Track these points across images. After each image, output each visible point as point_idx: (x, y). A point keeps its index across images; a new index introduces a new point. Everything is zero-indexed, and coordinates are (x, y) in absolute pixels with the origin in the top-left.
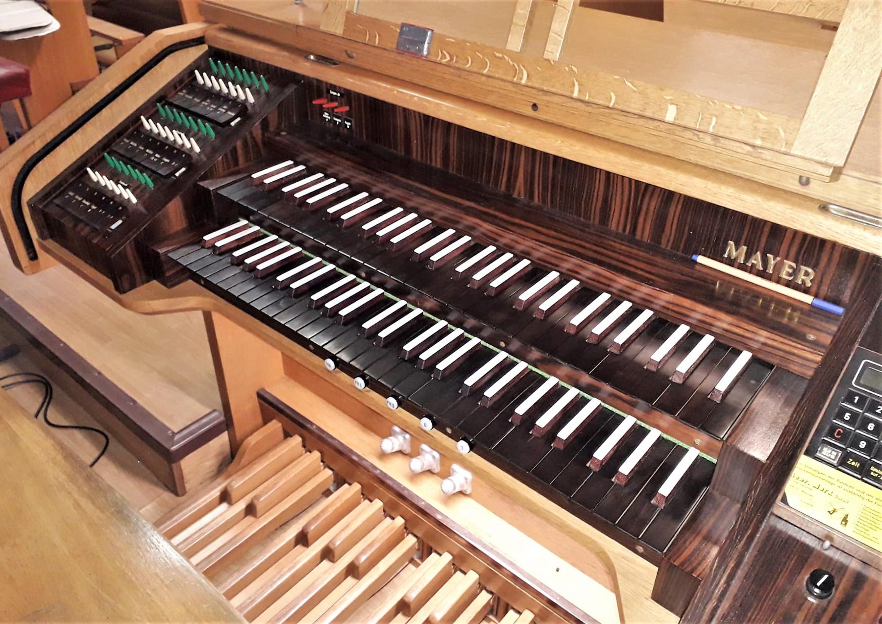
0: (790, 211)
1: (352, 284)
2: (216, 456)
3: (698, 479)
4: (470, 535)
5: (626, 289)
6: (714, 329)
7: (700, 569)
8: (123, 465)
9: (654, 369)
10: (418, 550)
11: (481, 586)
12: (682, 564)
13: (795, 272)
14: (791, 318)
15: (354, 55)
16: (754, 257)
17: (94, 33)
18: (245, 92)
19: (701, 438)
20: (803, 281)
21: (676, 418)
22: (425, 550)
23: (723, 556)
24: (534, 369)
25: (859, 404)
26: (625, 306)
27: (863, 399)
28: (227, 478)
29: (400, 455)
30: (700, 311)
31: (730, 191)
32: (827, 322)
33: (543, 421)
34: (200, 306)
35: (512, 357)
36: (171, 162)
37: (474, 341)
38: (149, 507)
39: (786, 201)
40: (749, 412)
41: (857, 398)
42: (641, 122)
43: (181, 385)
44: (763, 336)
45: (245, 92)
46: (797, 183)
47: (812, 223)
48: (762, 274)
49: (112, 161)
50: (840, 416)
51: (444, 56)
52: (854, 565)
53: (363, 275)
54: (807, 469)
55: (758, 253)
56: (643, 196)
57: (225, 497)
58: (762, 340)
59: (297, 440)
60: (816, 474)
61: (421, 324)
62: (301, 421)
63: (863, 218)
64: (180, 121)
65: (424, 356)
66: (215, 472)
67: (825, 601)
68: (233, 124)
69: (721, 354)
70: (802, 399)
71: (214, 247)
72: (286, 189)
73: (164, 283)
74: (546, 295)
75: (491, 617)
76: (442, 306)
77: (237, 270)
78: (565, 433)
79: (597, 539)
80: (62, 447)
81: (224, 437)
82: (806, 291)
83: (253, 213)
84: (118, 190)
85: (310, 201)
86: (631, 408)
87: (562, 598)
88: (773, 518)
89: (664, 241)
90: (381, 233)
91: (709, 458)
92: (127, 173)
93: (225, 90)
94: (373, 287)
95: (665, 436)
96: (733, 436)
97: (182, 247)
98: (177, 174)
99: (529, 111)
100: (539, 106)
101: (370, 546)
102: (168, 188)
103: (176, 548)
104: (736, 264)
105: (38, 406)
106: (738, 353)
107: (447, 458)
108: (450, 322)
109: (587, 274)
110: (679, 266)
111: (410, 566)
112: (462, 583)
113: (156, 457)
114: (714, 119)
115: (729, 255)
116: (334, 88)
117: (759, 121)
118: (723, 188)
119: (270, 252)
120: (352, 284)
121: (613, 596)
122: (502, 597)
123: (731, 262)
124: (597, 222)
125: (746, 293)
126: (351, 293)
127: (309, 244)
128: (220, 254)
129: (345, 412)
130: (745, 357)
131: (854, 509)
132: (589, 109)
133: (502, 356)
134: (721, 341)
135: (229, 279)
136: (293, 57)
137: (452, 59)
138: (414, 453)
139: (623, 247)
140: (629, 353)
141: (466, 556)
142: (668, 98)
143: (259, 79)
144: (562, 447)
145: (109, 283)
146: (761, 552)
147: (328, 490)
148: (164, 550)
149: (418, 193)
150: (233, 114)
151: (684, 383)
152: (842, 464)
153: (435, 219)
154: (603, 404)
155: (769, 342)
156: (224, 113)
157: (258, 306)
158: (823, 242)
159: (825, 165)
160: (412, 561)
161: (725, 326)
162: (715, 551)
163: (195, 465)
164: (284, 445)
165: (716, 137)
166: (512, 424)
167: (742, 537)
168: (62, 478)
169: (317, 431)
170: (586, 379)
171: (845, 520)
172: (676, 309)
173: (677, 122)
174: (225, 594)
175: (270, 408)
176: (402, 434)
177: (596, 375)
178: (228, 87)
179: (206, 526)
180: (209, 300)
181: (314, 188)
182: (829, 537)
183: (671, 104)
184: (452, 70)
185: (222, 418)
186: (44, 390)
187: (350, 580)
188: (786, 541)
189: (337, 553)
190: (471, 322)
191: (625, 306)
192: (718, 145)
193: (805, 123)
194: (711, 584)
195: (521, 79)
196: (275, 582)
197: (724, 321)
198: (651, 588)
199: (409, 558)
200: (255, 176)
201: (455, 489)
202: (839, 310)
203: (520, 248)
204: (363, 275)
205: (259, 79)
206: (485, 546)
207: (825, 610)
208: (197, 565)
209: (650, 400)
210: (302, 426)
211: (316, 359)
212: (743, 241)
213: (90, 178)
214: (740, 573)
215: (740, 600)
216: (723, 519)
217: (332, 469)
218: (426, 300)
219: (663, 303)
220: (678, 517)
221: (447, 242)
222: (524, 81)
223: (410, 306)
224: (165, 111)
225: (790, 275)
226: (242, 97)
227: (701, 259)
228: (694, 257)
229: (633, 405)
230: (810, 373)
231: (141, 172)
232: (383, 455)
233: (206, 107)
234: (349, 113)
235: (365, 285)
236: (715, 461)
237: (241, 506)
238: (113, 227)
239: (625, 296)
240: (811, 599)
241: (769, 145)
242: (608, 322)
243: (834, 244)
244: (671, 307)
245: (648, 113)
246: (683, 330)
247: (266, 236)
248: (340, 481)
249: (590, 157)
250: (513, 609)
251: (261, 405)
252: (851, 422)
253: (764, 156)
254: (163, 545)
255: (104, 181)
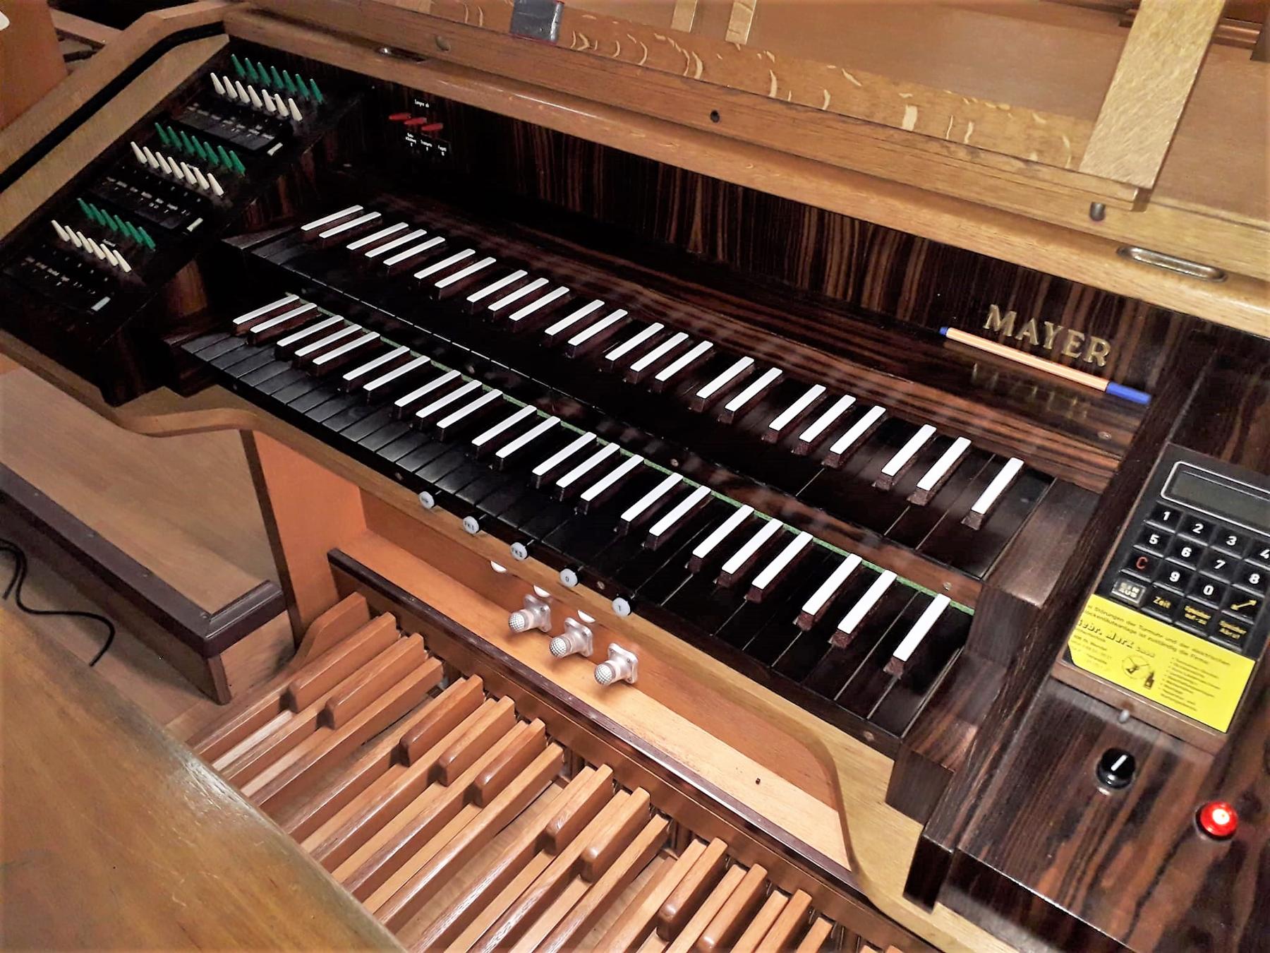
0: (1075, 257)
1: (456, 384)
2: (273, 646)
3: (950, 632)
4: (636, 739)
5: (846, 379)
6: (970, 430)
7: (954, 756)
8: (136, 664)
9: (887, 487)
10: (565, 763)
11: (652, 809)
12: (927, 752)
13: (1083, 347)
14: (1077, 413)
15: (449, 46)
16: (1025, 327)
17: (63, 36)
18: (287, 105)
19: (953, 580)
20: (1094, 358)
21: (916, 553)
22: (573, 764)
23: (983, 739)
24: (719, 496)
25: (1171, 522)
26: (846, 402)
27: (1175, 515)
28: (289, 676)
29: (536, 634)
30: (952, 405)
31: (993, 231)
32: (1128, 415)
33: (732, 566)
34: (235, 422)
35: (688, 481)
36: (180, 209)
37: (636, 460)
38: (178, 721)
39: (1071, 244)
40: (1018, 543)
41: (1167, 514)
42: (867, 130)
43: (219, 548)
44: (1039, 436)
45: (287, 105)
46: (1087, 217)
47: (1107, 273)
48: (1038, 351)
49: (91, 211)
50: (1145, 540)
51: (580, 42)
52: (1162, 742)
53: (472, 370)
54: (1098, 613)
55: (1033, 321)
56: (872, 244)
57: (287, 702)
58: (1038, 441)
59: (388, 619)
60: (1111, 619)
61: (556, 440)
62: (393, 592)
63: (1178, 265)
64: (191, 150)
65: (564, 482)
66: (271, 663)
67: (1122, 792)
68: (271, 152)
69: (978, 466)
70: (1091, 520)
71: (250, 335)
72: (352, 246)
73: (176, 389)
74: (737, 388)
75: (667, 850)
76: (586, 410)
77: (285, 367)
78: (762, 580)
79: (808, 725)
80: (37, 633)
81: (283, 619)
82: (1098, 373)
83: (307, 284)
84: (102, 252)
85: (389, 262)
86: (854, 544)
87: (765, 820)
88: (1052, 682)
89: (900, 312)
90: (494, 307)
91: (963, 608)
92: (114, 228)
93: (258, 103)
94: (485, 387)
95: (902, 580)
96: (997, 574)
97: (200, 336)
98: (190, 228)
99: (706, 123)
100: (722, 115)
101: (497, 761)
102: (174, 248)
103: (220, 774)
104: (1002, 339)
105: (8, 582)
106: (1002, 462)
107: (603, 632)
108: (599, 435)
109: (794, 359)
110: (925, 346)
111: (555, 785)
112: (627, 805)
113: (182, 647)
114: (971, 126)
115: (992, 327)
116: (420, 95)
117: (1033, 126)
118: (983, 227)
119: (330, 340)
120: (456, 384)
121: (834, 814)
122: (683, 823)
123: (993, 336)
124: (806, 285)
125: (1017, 379)
126: (453, 397)
127: (391, 325)
128: (259, 345)
129: (455, 578)
130: (1013, 466)
131: (1162, 664)
132: (793, 113)
133: (674, 479)
134: (979, 446)
135: (272, 379)
136: (360, 50)
137: (592, 45)
138: (559, 629)
139: (843, 320)
140: (851, 467)
141: (634, 766)
142: (906, 96)
143: (309, 86)
144: (758, 599)
145: (95, 392)
146: (1034, 731)
147: (436, 687)
148: (206, 781)
149: (551, 249)
150: (271, 138)
151: (929, 503)
152: (1146, 605)
153: (574, 285)
154: (815, 540)
155: (1047, 444)
156: (257, 137)
157: (317, 417)
158: (1122, 300)
159: (1128, 186)
160: (557, 780)
161: (985, 424)
162: (972, 731)
163: (242, 660)
164: (370, 627)
165: (973, 149)
166: (688, 572)
167: (1010, 708)
168: (39, 675)
169: (417, 606)
170: (793, 505)
171: (1150, 680)
172: (917, 403)
173: (918, 131)
174: (355, 894)
175: (348, 575)
176: (538, 605)
177: (806, 499)
178: (261, 98)
179: (260, 743)
180: (244, 413)
181: (394, 244)
182: (1128, 705)
183: (911, 104)
184: (592, 60)
185: (279, 592)
186: (14, 563)
187: (470, 810)
188: (1069, 716)
189: (450, 773)
190: (631, 433)
191: (846, 402)
192: (978, 160)
193: (1100, 126)
194: (968, 776)
195: (694, 73)
196: (363, 817)
197: (986, 418)
198: (885, 788)
199: (553, 775)
200: (306, 228)
201: (614, 676)
202: (1143, 398)
203: (699, 324)
204: (472, 370)
205: (309, 86)
206: (657, 753)
207: (1121, 804)
208: (251, 797)
209: (879, 529)
210: (397, 600)
211: (406, 493)
212: (1010, 305)
213: (56, 235)
214: (1007, 759)
215: (1007, 796)
216: (986, 685)
217: (440, 659)
218: (564, 404)
219: (900, 397)
220: (920, 689)
221: (592, 319)
222: (697, 76)
223: (541, 413)
224: (167, 135)
225: (1075, 350)
226: (285, 112)
227: (952, 333)
228: (942, 330)
229: (858, 539)
230: (1103, 485)
231: (136, 226)
232: (513, 636)
233: (228, 128)
234: (442, 133)
235: (475, 384)
236: (971, 612)
237: (311, 713)
238: (97, 307)
239: (847, 387)
240: (1104, 791)
241: (1047, 161)
242: (826, 422)
243: (1138, 303)
244: (910, 400)
245: (877, 119)
246: (926, 432)
247: (326, 317)
248: (452, 675)
249: (794, 189)
250: (698, 837)
251: (334, 572)
252: (1160, 546)
253: (1040, 175)
254: (204, 772)
255: (79, 239)
